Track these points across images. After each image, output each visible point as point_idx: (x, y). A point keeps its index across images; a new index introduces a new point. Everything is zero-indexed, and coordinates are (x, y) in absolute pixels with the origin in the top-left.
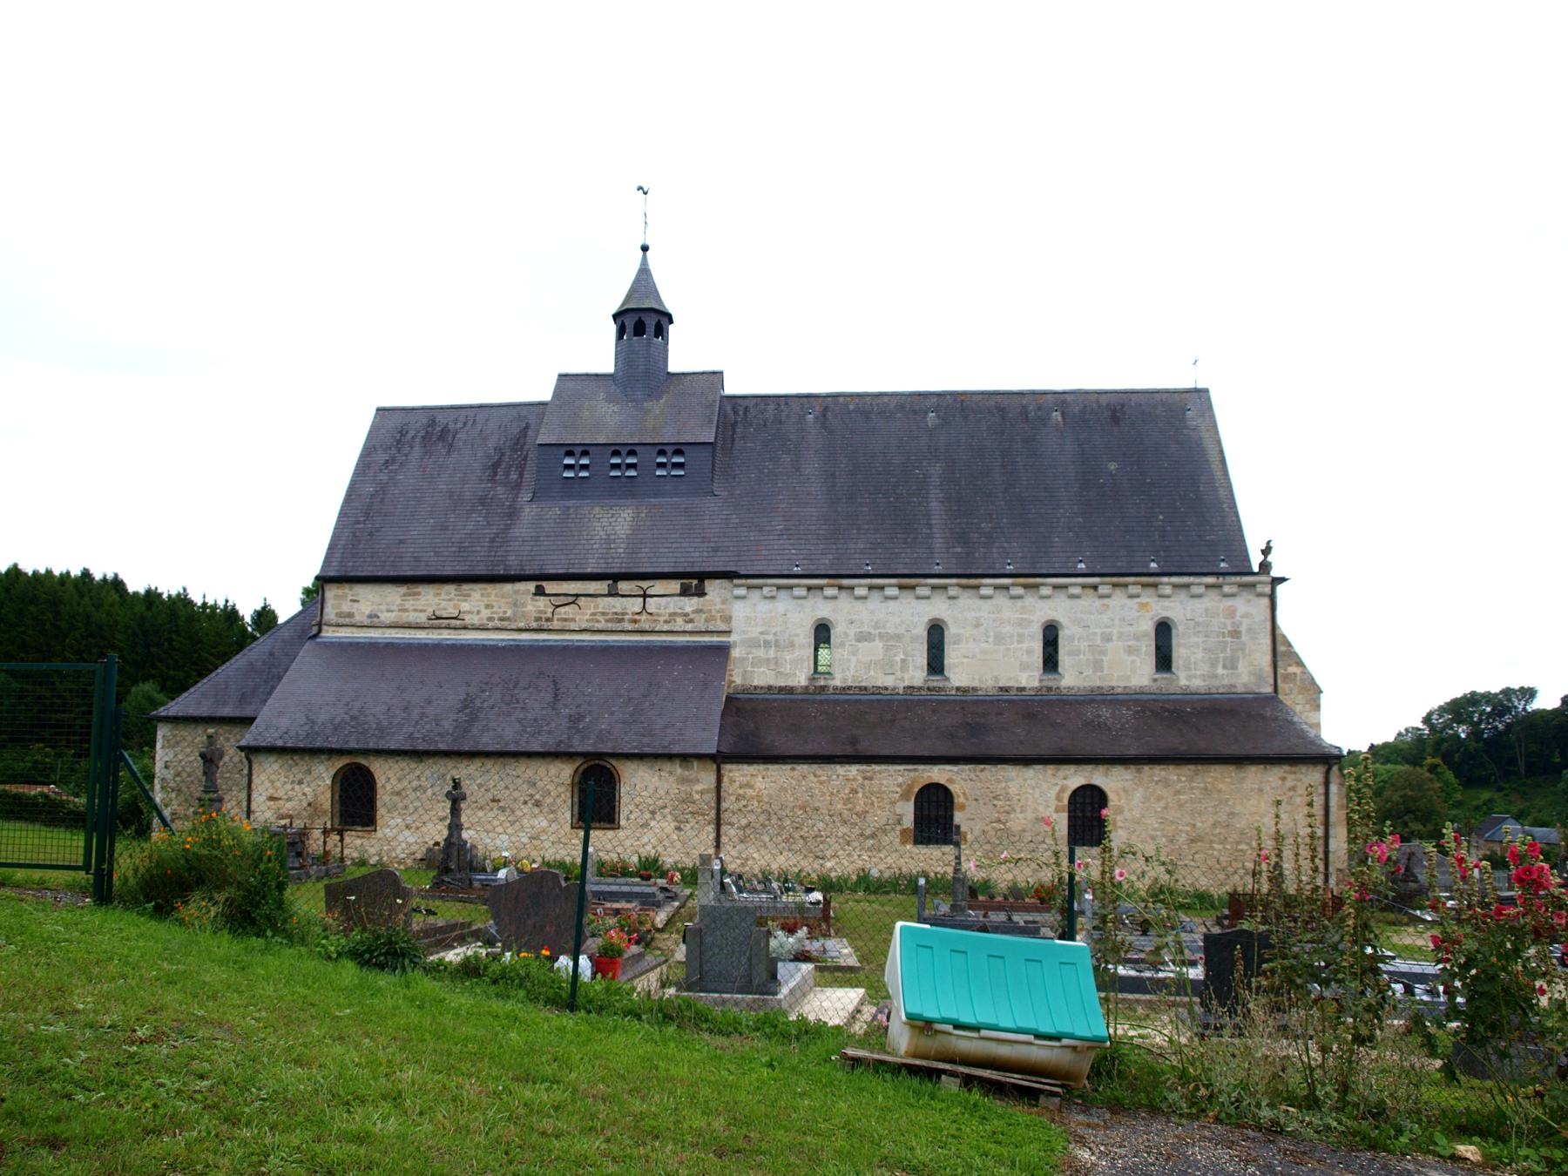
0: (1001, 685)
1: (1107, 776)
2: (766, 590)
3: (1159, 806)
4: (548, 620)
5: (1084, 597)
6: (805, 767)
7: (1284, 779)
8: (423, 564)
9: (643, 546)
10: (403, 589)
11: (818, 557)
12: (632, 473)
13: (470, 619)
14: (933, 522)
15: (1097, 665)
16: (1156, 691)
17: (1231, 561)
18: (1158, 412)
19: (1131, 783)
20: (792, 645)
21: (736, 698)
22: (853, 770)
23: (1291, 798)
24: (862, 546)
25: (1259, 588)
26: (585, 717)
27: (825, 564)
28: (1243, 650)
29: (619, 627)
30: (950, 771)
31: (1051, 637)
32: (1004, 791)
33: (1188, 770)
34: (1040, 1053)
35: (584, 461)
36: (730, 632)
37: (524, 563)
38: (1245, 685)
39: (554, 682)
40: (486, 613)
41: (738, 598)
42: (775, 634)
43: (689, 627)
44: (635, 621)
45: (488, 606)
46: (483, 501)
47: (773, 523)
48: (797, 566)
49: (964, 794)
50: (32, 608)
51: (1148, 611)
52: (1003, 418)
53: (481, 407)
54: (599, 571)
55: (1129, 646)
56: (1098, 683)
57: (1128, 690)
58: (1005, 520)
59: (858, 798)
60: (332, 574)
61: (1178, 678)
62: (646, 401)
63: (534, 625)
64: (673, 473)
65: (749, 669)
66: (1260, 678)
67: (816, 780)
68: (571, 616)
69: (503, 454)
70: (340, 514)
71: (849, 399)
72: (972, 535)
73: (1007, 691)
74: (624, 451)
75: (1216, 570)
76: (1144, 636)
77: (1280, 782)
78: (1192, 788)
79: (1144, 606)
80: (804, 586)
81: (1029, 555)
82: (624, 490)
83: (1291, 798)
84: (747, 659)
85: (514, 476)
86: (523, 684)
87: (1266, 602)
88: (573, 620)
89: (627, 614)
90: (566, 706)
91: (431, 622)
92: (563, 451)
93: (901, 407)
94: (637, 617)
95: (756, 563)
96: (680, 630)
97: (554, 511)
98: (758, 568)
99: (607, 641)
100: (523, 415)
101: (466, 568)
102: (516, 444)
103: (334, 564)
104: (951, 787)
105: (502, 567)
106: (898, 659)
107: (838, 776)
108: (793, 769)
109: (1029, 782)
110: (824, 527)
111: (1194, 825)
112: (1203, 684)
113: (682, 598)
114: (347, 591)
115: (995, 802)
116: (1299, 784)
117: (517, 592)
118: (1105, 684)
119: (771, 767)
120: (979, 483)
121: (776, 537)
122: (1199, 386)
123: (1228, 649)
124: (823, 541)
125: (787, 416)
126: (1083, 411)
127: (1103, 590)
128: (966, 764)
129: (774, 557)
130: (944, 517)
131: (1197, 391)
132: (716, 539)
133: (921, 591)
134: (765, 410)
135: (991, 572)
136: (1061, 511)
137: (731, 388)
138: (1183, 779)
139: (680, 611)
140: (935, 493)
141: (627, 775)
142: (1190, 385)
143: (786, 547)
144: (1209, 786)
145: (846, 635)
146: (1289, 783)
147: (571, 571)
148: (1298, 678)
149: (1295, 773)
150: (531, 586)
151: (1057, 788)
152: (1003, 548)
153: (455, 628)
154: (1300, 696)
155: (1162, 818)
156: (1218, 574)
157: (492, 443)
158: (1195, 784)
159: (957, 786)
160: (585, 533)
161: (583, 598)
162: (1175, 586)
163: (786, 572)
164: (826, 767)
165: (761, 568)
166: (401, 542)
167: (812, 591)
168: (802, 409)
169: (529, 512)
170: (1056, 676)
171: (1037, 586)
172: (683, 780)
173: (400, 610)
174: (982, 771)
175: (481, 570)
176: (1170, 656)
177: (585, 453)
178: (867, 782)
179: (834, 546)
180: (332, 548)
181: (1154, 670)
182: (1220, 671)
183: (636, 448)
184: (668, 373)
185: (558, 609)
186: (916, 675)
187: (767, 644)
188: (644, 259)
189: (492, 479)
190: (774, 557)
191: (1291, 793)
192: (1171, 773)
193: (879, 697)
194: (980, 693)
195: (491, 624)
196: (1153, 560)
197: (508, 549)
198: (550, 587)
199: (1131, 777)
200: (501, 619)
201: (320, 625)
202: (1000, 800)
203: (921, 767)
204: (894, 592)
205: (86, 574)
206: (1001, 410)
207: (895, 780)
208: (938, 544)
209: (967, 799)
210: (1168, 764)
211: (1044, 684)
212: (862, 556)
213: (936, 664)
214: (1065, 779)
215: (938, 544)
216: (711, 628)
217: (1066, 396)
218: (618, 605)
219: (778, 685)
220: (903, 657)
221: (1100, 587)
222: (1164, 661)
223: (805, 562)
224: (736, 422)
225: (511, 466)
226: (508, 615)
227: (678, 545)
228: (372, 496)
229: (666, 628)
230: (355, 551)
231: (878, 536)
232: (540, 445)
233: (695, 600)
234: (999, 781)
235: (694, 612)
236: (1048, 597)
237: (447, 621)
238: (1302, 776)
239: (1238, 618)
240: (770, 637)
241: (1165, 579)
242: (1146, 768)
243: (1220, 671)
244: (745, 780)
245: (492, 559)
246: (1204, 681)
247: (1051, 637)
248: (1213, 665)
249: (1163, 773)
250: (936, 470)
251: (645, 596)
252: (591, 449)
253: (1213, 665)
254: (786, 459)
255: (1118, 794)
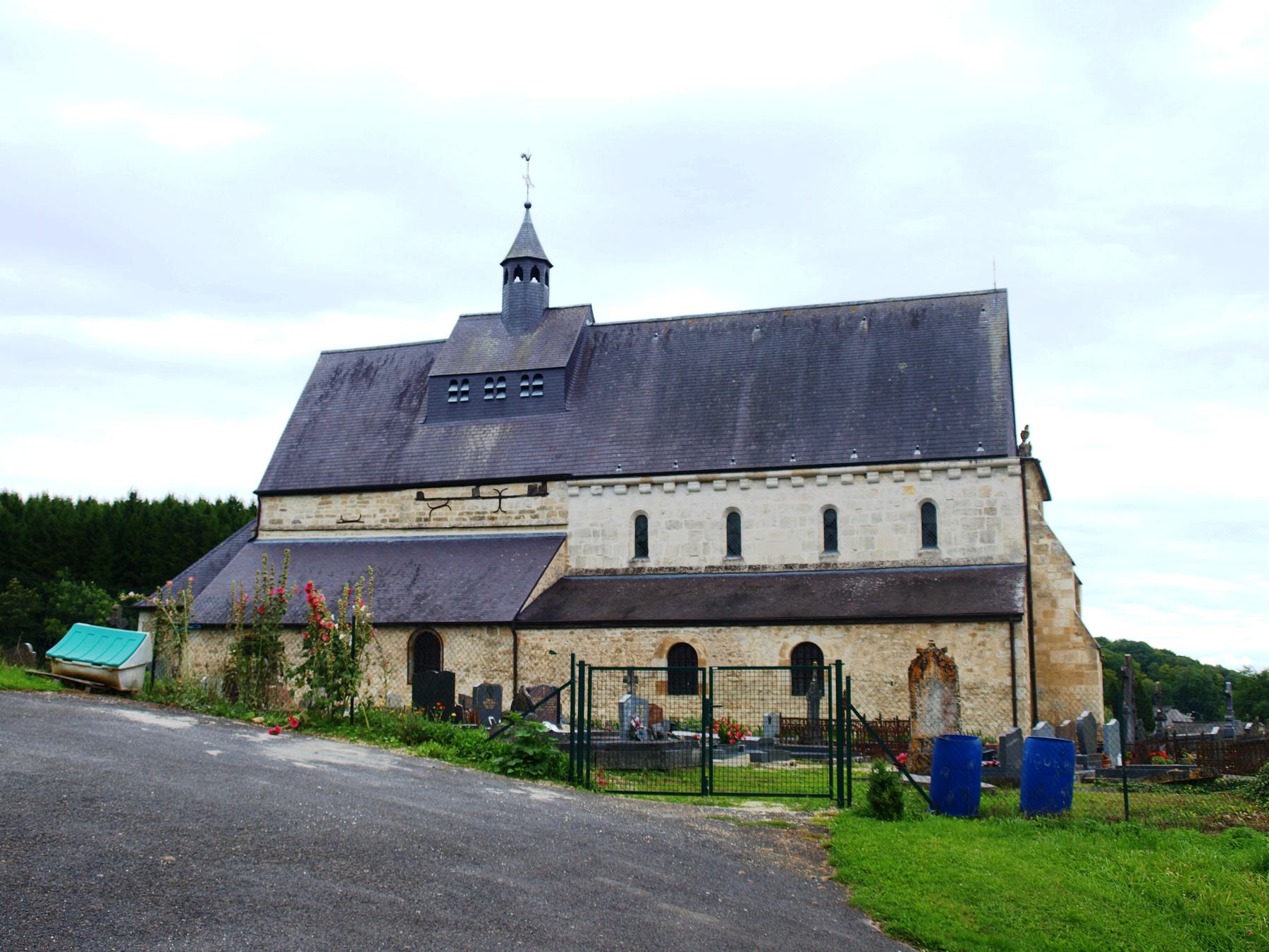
0: (786, 563)
1: (820, 635)
2: (593, 488)
3: (866, 660)
4: (426, 520)
5: (856, 483)
6: (581, 631)
7: (974, 635)
8: (334, 478)
9: (502, 456)
10: (318, 500)
11: (638, 458)
12: (502, 396)
13: (368, 522)
14: (738, 424)
15: (869, 543)
16: (920, 564)
17: (988, 446)
18: (955, 314)
19: (841, 640)
20: (616, 534)
21: (571, 580)
22: (618, 633)
23: (981, 651)
24: (675, 448)
25: (1010, 469)
26: (428, 596)
27: (642, 464)
28: (998, 525)
29: (480, 523)
30: (693, 632)
31: (830, 519)
32: (737, 649)
33: (889, 628)
34: (95, 671)
35: (465, 388)
36: (566, 525)
37: (410, 474)
38: (1000, 556)
39: (418, 570)
40: (380, 516)
41: (572, 496)
42: (602, 525)
43: (534, 522)
44: (493, 519)
45: (381, 511)
46: (388, 425)
47: (608, 432)
48: (619, 467)
49: (705, 652)
50: (177, 535)
51: (912, 493)
52: (816, 330)
53: (400, 346)
54: (465, 478)
55: (897, 526)
56: (869, 559)
57: (895, 565)
58: (798, 420)
59: (622, 657)
60: (266, 489)
61: (940, 553)
62: (522, 335)
63: (416, 524)
64: (534, 394)
65: (582, 555)
66: (1015, 550)
67: (589, 641)
68: (443, 516)
69: (409, 386)
70: (281, 441)
71: (690, 321)
72: (768, 434)
73: (791, 568)
74: (495, 378)
75: (971, 454)
76: (910, 516)
77: (970, 638)
78: (894, 644)
79: (909, 488)
80: (623, 484)
81: (812, 449)
82: (495, 410)
83: (981, 651)
84: (580, 547)
85: (415, 403)
86: (394, 572)
87: (1018, 480)
88: (446, 519)
89: (486, 513)
90: (418, 587)
91: (339, 525)
92: (448, 381)
93: (732, 326)
94: (494, 515)
95: (587, 466)
96: (526, 524)
97: (440, 430)
98: (586, 470)
99: (471, 536)
100: (429, 349)
101: (366, 480)
102: (421, 377)
103: (270, 481)
104: (694, 646)
105: (393, 478)
106: (701, 543)
107: (606, 638)
108: (572, 633)
109: (756, 641)
110: (648, 433)
111: (897, 677)
112: (962, 557)
113: (530, 498)
114: (278, 502)
115: (730, 658)
116: (988, 639)
117: (403, 498)
118: (876, 559)
119: (555, 631)
120: (784, 388)
121: (608, 444)
122: (998, 287)
123: (985, 525)
124: (644, 446)
125: (637, 340)
126: (887, 319)
127: (871, 476)
128: (706, 626)
129: (602, 461)
130: (748, 419)
131: (996, 292)
132: (560, 448)
133: (718, 484)
134: (620, 336)
135: (777, 465)
136: (848, 409)
137: (600, 319)
138: (886, 636)
139: (527, 509)
140: (745, 398)
141: (448, 640)
142: (991, 287)
143: (614, 451)
144: (908, 642)
145: (658, 523)
146: (979, 639)
147: (444, 479)
148: (1050, 549)
149: (984, 630)
150: (414, 493)
151: (780, 646)
152: (792, 444)
153: (356, 529)
154: (1052, 566)
155: (869, 671)
156: (969, 458)
157: (402, 377)
158: (895, 641)
159: (699, 645)
160: (460, 448)
161: (453, 501)
162: (934, 470)
163: (609, 473)
164: (597, 630)
165: (590, 470)
166: (321, 461)
167: (631, 488)
168: (650, 332)
169: (421, 432)
170: (834, 554)
171: (814, 476)
172: (490, 644)
173: (316, 516)
174: (719, 632)
175: (377, 481)
176: (935, 533)
177: (465, 382)
178: (629, 643)
179: (652, 449)
180: (270, 468)
181: (921, 545)
182: (978, 544)
183: (505, 375)
184: (548, 309)
185: (434, 511)
186: (716, 555)
187: (595, 534)
188: (527, 214)
189: (398, 407)
190: (602, 461)
191: (981, 648)
192: (875, 632)
193: (684, 576)
194: (768, 570)
195: (384, 525)
196: (918, 449)
197: (400, 463)
198: (428, 493)
199: (841, 635)
200: (391, 521)
201: (257, 530)
202: (734, 656)
203: (670, 630)
204: (696, 485)
205: (46, 497)
206: (817, 322)
207: (651, 640)
208: (738, 443)
209: (707, 656)
210: (872, 624)
211: (823, 561)
212: (673, 456)
213: (734, 547)
214: (786, 637)
215: (738, 443)
216: (552, 522)
217: (876, 305)
218: (480, 506)
219: (605, 568)
220: (705, 541)
221: (868, 474)
222: (930, 537)
223: (627, 464)
224: (595, 347)
225: (414, 395)
226: (397, 517)
227: (530, 454)
228: (306, 425)
229: (516, 523)
230: (287, 470)
231: (690, 438)
232: (431, 377)
233: (540, 498)
234: (732, 640)
235: (538, 509)
236: (825, 485)
237: (350, 524)
238: (990, 633)
239: (993, 497)
240: (598, 528)
241: (923, 465)
242: (854, 627)
243: (978, 544)
244: (534, 643)
245: (386, 472)
246: (964, 554)
247: (830, 519)
248: (972, 540)
249: (868, 631)
250: (750, 379)
251: (500, 497)
252: (470, 378)
253: (972, 540)
254: (629, 376)
255: (831, 650)
